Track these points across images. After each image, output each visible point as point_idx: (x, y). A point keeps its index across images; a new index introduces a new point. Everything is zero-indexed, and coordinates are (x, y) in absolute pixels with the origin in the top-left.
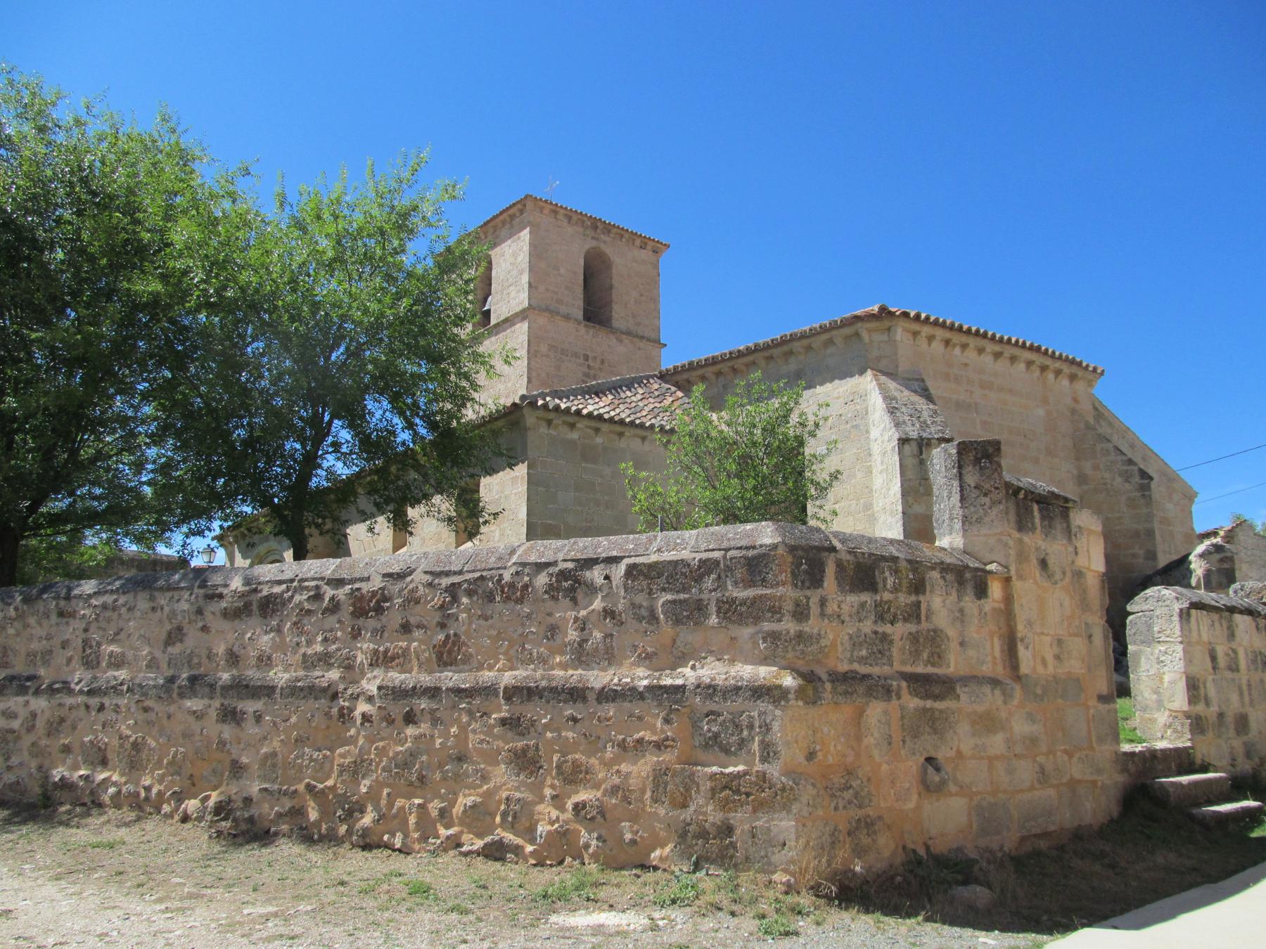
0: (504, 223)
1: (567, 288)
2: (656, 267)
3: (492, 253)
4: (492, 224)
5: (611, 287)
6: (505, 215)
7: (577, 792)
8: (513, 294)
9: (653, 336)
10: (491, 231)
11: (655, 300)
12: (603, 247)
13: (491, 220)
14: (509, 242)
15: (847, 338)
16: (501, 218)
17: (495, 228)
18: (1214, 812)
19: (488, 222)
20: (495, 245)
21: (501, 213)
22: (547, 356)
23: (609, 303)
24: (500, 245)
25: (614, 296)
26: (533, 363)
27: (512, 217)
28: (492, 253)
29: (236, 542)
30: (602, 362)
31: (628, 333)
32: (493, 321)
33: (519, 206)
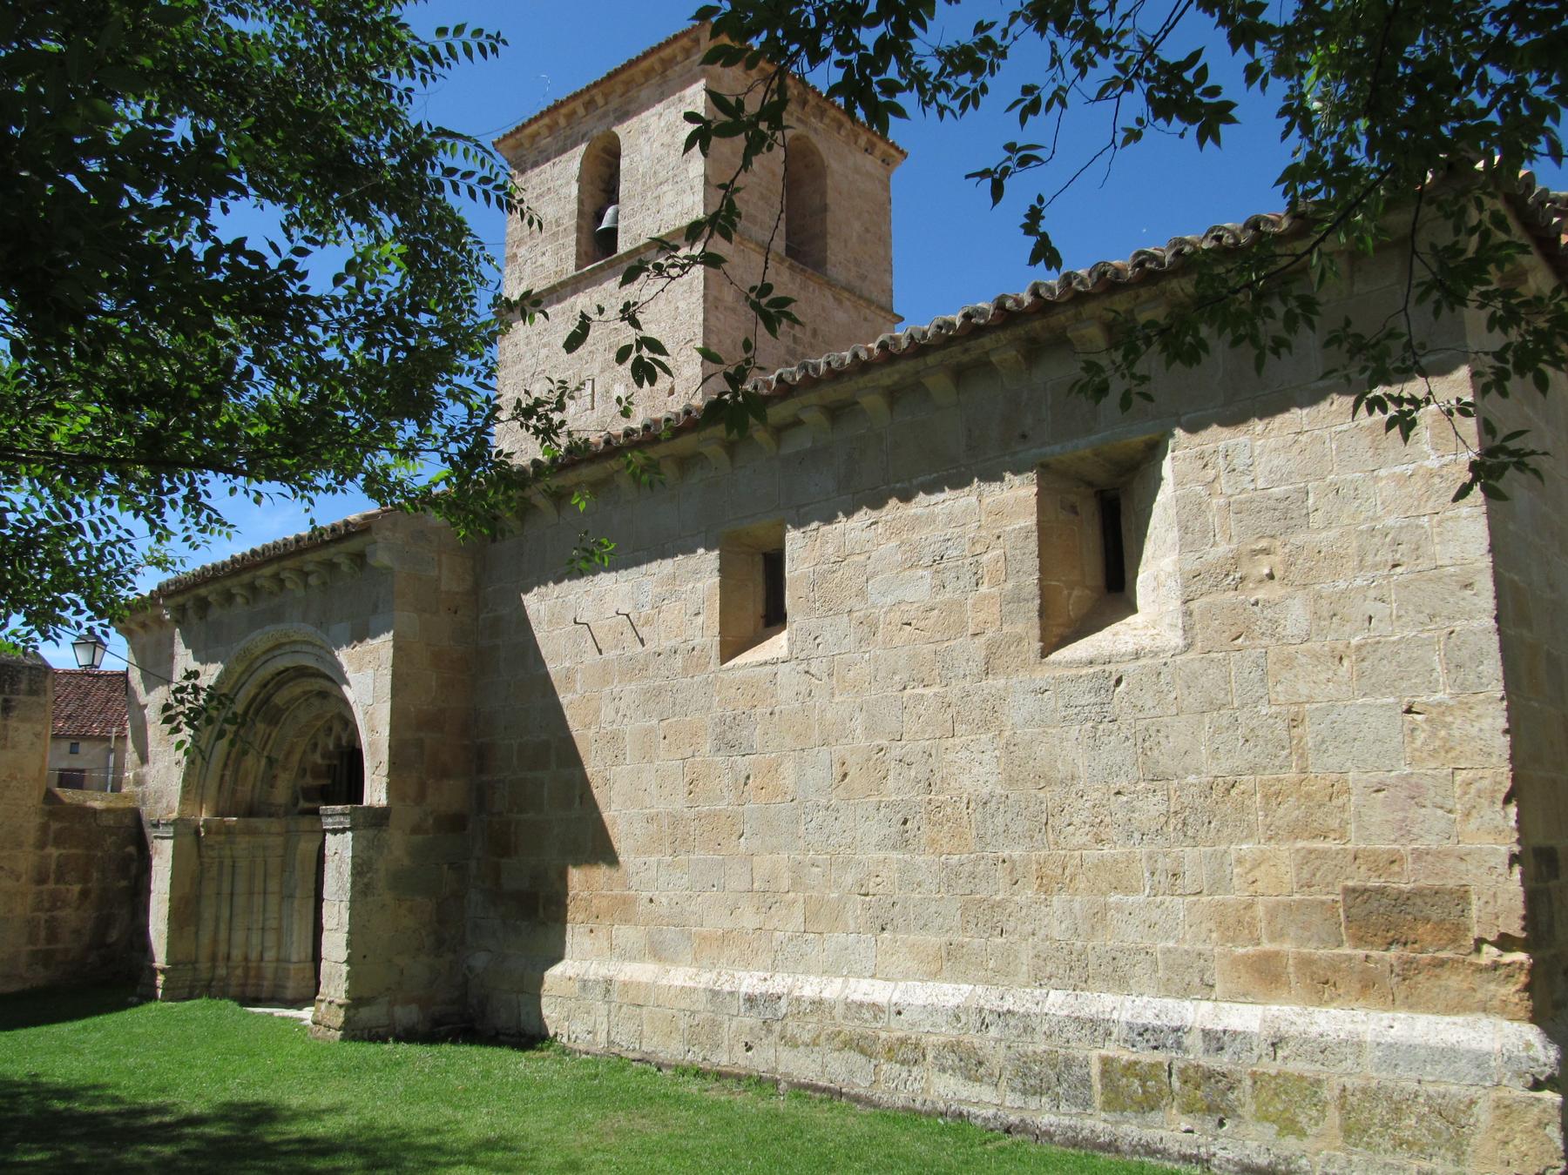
0: (647, 75)
1: (762, 197)
2: (886, 188)
3: (620, 130)
4: (623, 77)
5: (825, 208)
6: (676, 46)
7: (931, 1010)
8: (669, 198)
9: (883, 300)
10: (619, 89)
11: (884, 240)
12: (814, 138)
13: (624, 68)
14: (659, 107)
15: (893, 395)
16: (645, 64)
17: (628, 84)
18: (164, 941)
19: (617, 72)
20: (624, 115)
21: (646, 55)
22: (734, 310)
23: (823, 235)
24: (637, 112)
25: (830, 227)
26: (713, 320)
27: (667, 64)
28: (620, 130)
29: (178, 622)
30: (815, 333)
31: (849, 289)
32: (623, 247)
33: (685, 42)
